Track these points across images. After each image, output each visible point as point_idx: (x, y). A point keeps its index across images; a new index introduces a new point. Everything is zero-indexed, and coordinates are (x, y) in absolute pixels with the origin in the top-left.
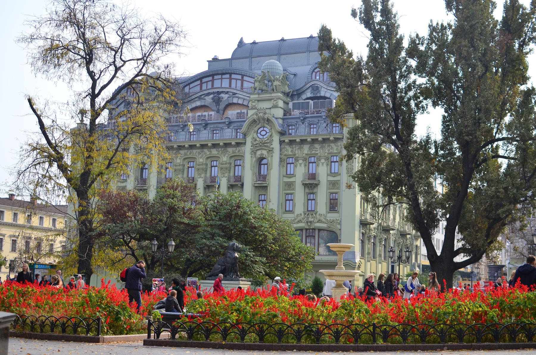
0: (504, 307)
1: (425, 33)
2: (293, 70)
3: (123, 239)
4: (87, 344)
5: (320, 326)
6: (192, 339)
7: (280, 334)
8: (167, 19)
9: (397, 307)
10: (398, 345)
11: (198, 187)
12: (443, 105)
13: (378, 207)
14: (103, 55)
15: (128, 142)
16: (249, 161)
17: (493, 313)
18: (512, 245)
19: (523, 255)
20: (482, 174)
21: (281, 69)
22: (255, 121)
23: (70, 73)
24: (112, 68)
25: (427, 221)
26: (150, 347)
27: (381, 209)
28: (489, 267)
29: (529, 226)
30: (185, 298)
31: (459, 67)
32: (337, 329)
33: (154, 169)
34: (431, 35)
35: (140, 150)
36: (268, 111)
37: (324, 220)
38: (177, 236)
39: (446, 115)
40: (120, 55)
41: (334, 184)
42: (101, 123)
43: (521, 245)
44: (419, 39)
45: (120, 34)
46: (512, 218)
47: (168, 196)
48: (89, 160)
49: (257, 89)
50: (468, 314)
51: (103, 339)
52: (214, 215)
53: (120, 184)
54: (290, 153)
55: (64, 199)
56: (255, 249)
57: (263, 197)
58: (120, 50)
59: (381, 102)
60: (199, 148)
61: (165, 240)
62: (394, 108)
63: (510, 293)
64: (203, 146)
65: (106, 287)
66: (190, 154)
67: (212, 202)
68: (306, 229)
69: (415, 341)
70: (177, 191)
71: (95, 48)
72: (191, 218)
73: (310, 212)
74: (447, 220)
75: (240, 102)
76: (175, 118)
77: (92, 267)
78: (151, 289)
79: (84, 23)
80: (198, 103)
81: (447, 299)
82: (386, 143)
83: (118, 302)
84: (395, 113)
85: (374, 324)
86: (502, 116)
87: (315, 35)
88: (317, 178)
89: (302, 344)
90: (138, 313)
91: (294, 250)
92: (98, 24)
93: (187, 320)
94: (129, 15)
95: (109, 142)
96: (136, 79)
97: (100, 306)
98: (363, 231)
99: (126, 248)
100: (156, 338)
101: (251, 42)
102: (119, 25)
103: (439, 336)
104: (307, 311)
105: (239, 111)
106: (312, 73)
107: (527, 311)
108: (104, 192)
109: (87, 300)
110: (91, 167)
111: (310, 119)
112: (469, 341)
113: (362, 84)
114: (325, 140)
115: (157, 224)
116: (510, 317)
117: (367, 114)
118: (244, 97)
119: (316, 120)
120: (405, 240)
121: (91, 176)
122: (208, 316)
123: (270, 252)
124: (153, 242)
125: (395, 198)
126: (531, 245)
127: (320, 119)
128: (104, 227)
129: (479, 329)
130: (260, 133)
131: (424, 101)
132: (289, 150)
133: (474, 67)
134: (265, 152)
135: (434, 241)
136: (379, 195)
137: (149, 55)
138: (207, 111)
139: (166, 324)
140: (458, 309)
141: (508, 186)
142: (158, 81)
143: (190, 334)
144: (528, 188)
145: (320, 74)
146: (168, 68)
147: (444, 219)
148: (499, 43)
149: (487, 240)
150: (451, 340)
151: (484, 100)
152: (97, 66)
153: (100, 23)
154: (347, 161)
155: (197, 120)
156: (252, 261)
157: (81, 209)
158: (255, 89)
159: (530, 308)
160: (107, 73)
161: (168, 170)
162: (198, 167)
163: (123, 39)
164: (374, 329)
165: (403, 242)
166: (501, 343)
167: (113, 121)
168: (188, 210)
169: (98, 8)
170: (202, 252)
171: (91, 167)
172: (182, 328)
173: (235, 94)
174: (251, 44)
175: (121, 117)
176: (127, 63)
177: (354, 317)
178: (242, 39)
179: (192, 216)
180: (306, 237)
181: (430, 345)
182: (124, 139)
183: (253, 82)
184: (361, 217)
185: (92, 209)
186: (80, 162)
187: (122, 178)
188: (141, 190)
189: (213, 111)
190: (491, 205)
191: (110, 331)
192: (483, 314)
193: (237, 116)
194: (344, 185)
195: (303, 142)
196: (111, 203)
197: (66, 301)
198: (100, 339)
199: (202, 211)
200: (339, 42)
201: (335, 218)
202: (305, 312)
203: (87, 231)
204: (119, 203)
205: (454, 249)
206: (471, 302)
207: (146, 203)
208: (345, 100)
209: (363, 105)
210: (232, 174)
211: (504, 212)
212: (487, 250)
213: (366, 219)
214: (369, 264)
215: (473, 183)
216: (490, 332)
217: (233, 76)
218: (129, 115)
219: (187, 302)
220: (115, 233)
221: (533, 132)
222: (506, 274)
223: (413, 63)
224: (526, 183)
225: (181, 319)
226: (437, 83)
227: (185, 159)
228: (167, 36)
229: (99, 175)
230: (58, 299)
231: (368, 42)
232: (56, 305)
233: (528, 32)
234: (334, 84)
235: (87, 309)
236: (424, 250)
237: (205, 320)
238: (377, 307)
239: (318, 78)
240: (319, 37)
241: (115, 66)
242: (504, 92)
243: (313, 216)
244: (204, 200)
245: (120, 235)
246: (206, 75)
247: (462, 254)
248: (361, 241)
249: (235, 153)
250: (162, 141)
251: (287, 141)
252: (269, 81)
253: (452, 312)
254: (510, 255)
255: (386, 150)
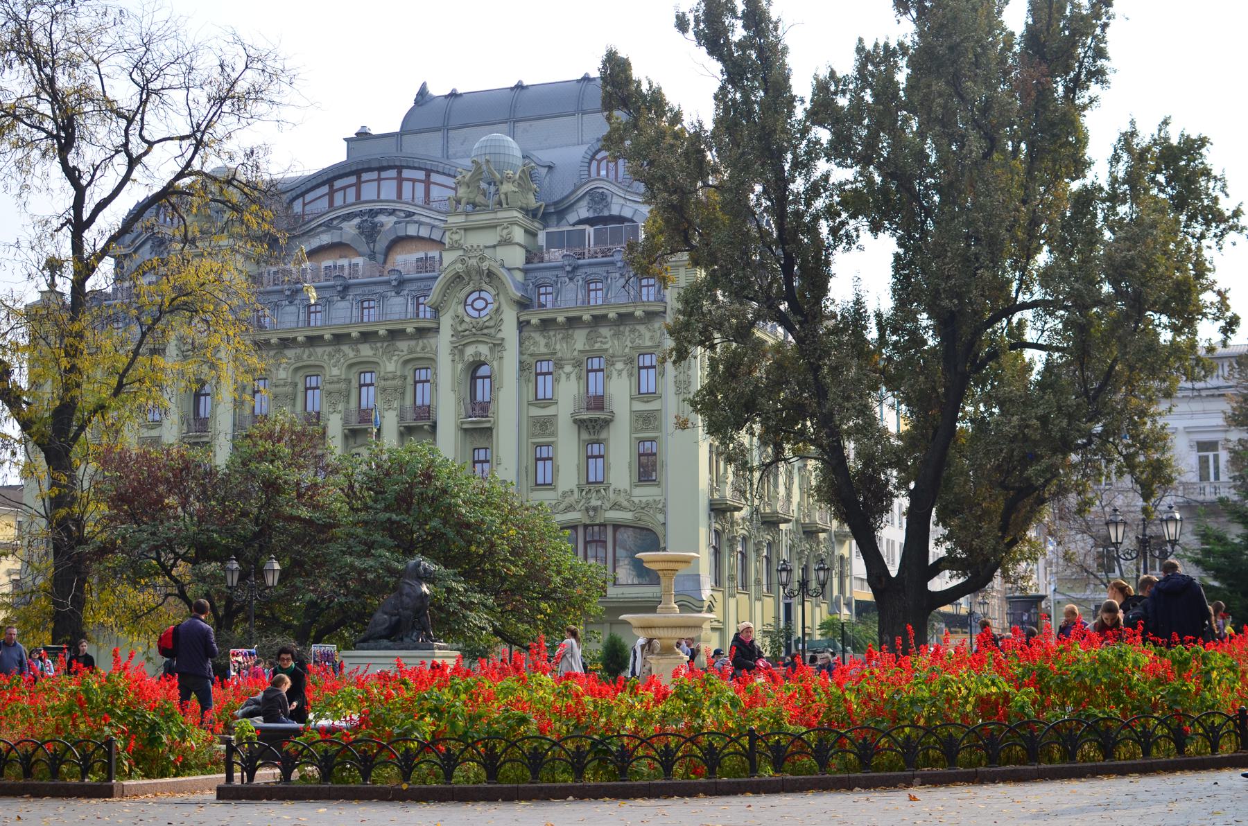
0: (1048, 682)
1: (847, 66)
2: (545, 156)
3: (158, 559)
4: (85, 801)
5: (626, 740)
6: (330, 780)
7: (536, 761)
8: (248, 41)
9: (804, 693)
10: (809, 777)
11: (330, 433)
12: (895, 230)
13: (751, 470)
14: (100, 129)
15: (163, 332)
16: (447, 371)
17: (1024, 697)
18: (1060, 548)
19: (1087, 571)
20: (989, 387)
21: (519, 155)
22: (459, 277)
23: (22, 172)
24: (122, 159)
25: (865, 499)
26: (233, 802)
27: (757, 475)
28: (1010, 600)
29: (1097, 503)
30: (309, 691)
31: (929, 141)
32: (667, 746)
33: (226, 394)
34: (861, 69)
35: (191, 350)
36: (488, 253)
37: (625, 503)
38: (283, 549)
39: (901, 251)
40: (138, 128)
41: (647, 420)
42: (98, 288)
43: (1082, 548)
44: (837, 82)
45: (139, 79)
46: (1059, 486)
47: (261, 457)
48: (71, 376)
49: (463, 201)
50: (967, 702)
51: (120, 787)
52: (371, 497)
53: (145, 433)
54: (543, 350)
55: (15, 471)
56: (467, 575)
57: (482, 455)
58: (138, 117)
59: (753, 228)
60: (329, 343)
61: (257, 560)
62: (782, 240)
63: (1061, 651)
64: (339, 339)
65: (125, 668)
66: (309, 357)
67: (364, 467)
68: (586, 526)
69: (847, 767)
70: (282, 443)
71: (80, 114)
72: (316, 507)
73: (593, 485)
74: (911, 494)
75: (424, 233)
76: (272, 275)
77: (85, 629)
78: (227, 675)
79: (53, 55)
80: (326, 239)
81: (916, 670)
82: (764, 321)
83: (155, 702)
84: (784, 250)
85: (751, 731)
86: (1030, 253)
87: (595, 74)
88: (606, 405)
89: (586, 783)
90: (201, 724)
91: (559, 573)
92: (85, 57)
93: (318, 737)
94: (158, 34)
95: (118, 333)
96: (177, 184)
97: (111, 713)
98: (718, 526)
99: (164, 581)
100: (246, 781)
101: (447, 93)
102: (136, 57)
103: (903, 754)
104: (596, 707)
105: (421, 255)
106: (590, 163)
107: (1099, 692)
108: (109, 450)
109: (80, 699)
110: (76, 392)
111: (588, 270)
112: (970, 764)
113: (706, 185)
114: (624, 318)
115: (236, 522)
116: (1063, 705)
117: (719, 255)
118: (432, 221)
119: (601, 271)
120: (814, 545)
121: (78, 414)
122: (367, 727)
123: (503, 579)
124: (229, 565)
125: (790, 446)
126: (1104, 547)
127: (610, 268)
128: (112, 533)
129: (992, 733)
130: (472, 305)
131: (852, 222)
132: (540, 343)
133: (962, 139)
134: (484, 350)
135: (882, 546)
136: (751, 441)
137: (206, 128)
138: (346, 257)
139: (269, 748)
140: (942, 692)
141: (1049, 413)
142: (231, 188)
143: (326, 770)
144: (1095, 416)
145: (608, 162)
146: (254, 157)
147: (903, 492)
148: (1020, 87)
149: (1003, 538)
150: (929, 762)
151: (984, 216)
152: (86, 156)
153: (90, 52)
154: (674, 363)
155: (322, 278)
156: (461, 603)
157: (57, 492)
158: (458, 202)
159: (1105, 683)
160: (110, 171)
161: (257, 395)
162: (328, 387)
163: (146, 92)
164: (752, 743)
165: (811, 549)
166: (1043, 766)
167: (126, 284)
168: (308, 489)
169: (85, 20)
170: (345, 585)
171: (76, 392)
172: (306, 756)
173: (410, 214)
174: (446, 97)
175: (144, 273)
176: (156, 146)
177: (704, 716)
178: (424, 86)
179: (319, 501)
180: (586, 543)
181: (882, 774)
182: (154, 324)
183: (454, 186)
184: (712, 494)
185: (83, 491)
186: (50, 382)
187: (150, 417)
188: (197, 444)
189: (360, 255)
190: (1010, 458)
191: (136, 769)
192: (1001, 701)
193: (418, 266)
194: (669, 422)
195: (573, 322)
196: (127, 477)
197: (31, 703)
198: (115, 789)
199: (342, 490)
200: (651, 87)
201: (651, 499)
202: (591, 708)
203: (73, 543)
204: (146, 475)
205: (928, 561)
206: (973, 672)
207: (211, 473)
208: (667, 221)
209: (708, 234)
210: (408, 402)
211: (1039, 474)
212: (1005, 561)
213: (723, 498)
214: (732, 602)
215: (969, 409)
216: (1018, 741)
217: (406, 173)
218: (163, 270)
219: (314, 700)
220: (139, 546)
221: (1101, 287)
222: (1050, 616)
223: (824, 135)
224: (1089, 404)
225: (302, 735)
226: (878, 179)
227: (297, 369)
228: (250, 81)
229: (95, 412)
230: (10, 699)
231: (715, 86)
232: (7, 715)
233: (1084, 57)
234: (642, 188)
235: (82, 719)
236: (859, 567)
237: (359, 736)
238: (757, 691)
239: (603, 173)
240: (604, 78)
241: (129, 155)
242: (1035, 197)
243: (600, 495)
244: (346, 464)
245: (150, 550)
246: (341, 172)
247: (947, 573)
248: (712, 550)
249: (415, 352)
250: (244, 329)
251: (534, 321)
252: (489, 184)
253: (931, 698)
254: (1057, 573)
255: (766, 338)
